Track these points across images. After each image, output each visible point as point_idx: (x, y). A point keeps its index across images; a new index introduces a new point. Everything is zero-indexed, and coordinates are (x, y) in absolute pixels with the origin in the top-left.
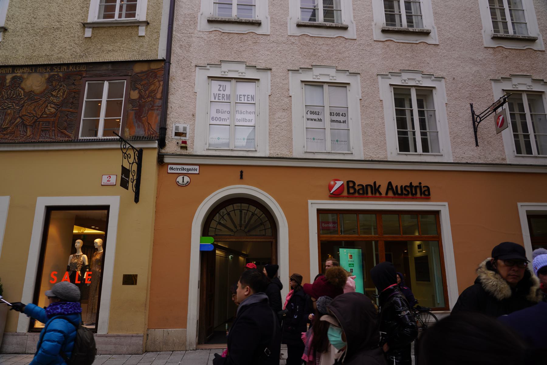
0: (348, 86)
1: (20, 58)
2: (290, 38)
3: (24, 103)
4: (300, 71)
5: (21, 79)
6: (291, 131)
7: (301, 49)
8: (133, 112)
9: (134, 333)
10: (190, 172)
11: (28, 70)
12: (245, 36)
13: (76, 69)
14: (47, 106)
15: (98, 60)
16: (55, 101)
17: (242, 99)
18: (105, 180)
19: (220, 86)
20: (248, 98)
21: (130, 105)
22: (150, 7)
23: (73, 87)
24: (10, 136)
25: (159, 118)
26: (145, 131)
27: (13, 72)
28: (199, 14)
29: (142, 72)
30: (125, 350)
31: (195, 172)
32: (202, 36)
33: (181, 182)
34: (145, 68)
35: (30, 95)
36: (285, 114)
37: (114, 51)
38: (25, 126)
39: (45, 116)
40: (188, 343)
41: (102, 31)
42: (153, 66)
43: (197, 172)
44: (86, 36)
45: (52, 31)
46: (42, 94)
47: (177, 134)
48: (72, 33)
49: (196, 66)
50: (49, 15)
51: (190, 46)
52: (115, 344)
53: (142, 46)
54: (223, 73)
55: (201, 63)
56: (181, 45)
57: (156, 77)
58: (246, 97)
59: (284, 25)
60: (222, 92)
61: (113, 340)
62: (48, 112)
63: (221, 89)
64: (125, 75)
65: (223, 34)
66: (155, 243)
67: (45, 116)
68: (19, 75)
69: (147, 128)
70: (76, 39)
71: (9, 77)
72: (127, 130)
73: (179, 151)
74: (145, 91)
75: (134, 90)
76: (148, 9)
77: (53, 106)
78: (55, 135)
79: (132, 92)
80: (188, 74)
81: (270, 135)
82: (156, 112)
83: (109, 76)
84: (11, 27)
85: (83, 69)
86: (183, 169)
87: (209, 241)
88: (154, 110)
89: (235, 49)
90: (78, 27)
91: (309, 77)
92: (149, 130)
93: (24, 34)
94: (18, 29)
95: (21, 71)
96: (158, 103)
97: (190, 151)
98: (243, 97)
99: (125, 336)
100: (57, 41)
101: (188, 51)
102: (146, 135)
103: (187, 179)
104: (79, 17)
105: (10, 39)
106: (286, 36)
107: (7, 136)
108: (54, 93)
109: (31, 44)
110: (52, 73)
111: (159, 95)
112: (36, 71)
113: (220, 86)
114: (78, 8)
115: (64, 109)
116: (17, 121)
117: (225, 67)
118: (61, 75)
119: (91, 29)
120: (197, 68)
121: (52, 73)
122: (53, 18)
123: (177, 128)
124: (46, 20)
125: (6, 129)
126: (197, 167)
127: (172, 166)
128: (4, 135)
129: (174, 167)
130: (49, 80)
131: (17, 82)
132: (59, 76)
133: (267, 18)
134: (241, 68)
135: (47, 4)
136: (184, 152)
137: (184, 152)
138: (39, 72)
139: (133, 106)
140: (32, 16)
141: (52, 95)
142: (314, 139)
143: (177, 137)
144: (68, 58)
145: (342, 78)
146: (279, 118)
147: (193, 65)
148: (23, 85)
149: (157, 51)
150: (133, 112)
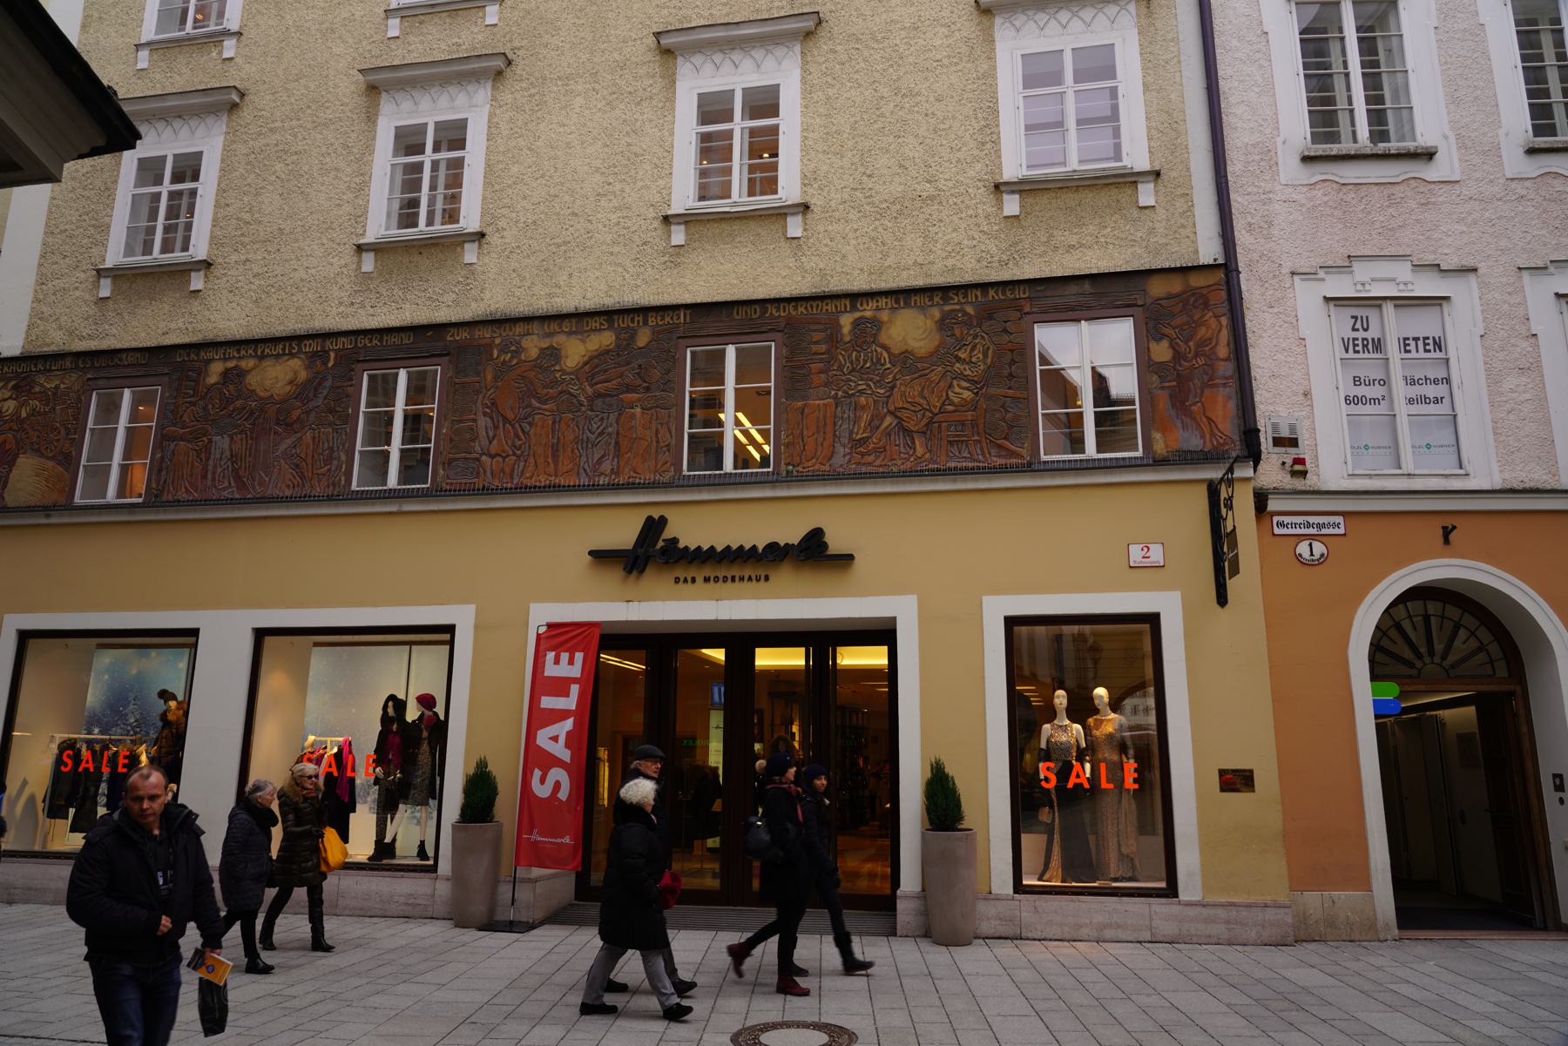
0: (1445, 304)
1: (853, 271)
2: (1514, 185)
3: (895, 379)
4: (1552, 269)
5: (877, 324)
6: (1547, 422)
7: (1545, 211)
8: (1166, 392)
9: (1268, 899)
10: (1324, 531)
11: (890, 302)
12: (1398, 188)
13: (1004, 293)
14: (951, 386)
15: (1047, 274)
16: (968, 372)
17: (1412, 347)
18: (1136, 554)
19: (1355, 318)
20: (1425, 344)
21: (1155, 377)
22: (1154, 132)
23: (1006, 338)
24: (877, 457)
25: (1232, 405)
26: (1203, 437)
27: (854, 308)
28: (1279, 141)
29: (1169, 297)
30: (1252, 935)
31: (1336, 531)
32: (1295, 196)
33: (1306, 555)
34: (1176, 285)
35: (906, 360)
36: (1524, 380)
37: (1082, 245)
38: (908, 433)
39: (950, 408)
40: (1380, 924)
41: (1044, 199)
42: (1196, 281)
43: (1342, 531)
44: (1007, 213)
45: (918, 204)
46: (934, 356)
47: (1278, 442)
48: (968, 207)
49: (1293, 273)
50: (901, 166)
51: (1270, 224)
52: (1228, 922)
53: (1152, 231)
54: (1359, 287)
55: (1303, 265)
56: (1250, 224)
57: (1206, 305)
58: (1420, 343)
59: (1495, 151)
60: (1361, 334)
61: (1220, 912)
62: (956, 400)
63: (1358, 325)
64: (1128, 306)
65: (1344, 189)
66: (1276, 700)
67: (950, 408)
68: (868, 314)
69: (1207, 431)
70: (981, 220)
71: (846, 321)
72: (1157, 436)
73: (1287, 482)
74: (1186, 343)
75: (1158, 340)
76: (1150, 139)
77: (965, 384)
78: (983, 453)
79: (1153, 345)
80: (1278, 294)
81: (1495, 434)
82: (1222, 393)
83: (1089, 308)
84: (816, 202)
85: (1022, 293)
86: (1309, 525)
87: (1391, 690)
88: (1215, 386)
89: (1378, 225)
90: (982, 194)
91: (1341, 286)
92: (1213, 435)
93: (851, 216)
94: (833, 204)
95: (872, 304)
96: (1226, 369)
97: (1311, 481)
98: (1413, 343)
99: (1249, 906)
100: (935, 229)
101: (1268, 238)
102: (1208, 447)
103: (1319, 548)
104: (979, 166)
105: (821, 228)
106: (1502, 181)
107: (871, 458)
108: (962, 355)
109: (873, 239)
110: (947, 308)
111: (1223, 351)
112: (907, 305)
113: (1355, 318)
114: (972, 144)
115: (992, 390)
116: (886, 424)
117: (1362, 271)
118: (970, 310)
119: (1017, 196)
120: (1296, 278)
121: (947, 308)
122: (914, 173)
123: (1275, 427)
124: (897, 179)
125: (863, 441)
126: (1340, 519)
127: (1281, 518)
128: (863, 455)
129: (1287, 519)
130: (943, 324)
131: (867, 331)
132: (965, 313)
133: (1446, 137)
134: (1403, 271)
135: (891, 139)
136: (1299, 484)
137: (1299, 484)
138: (915, 306)
139: (1162, 379)
140: (861, 169)
141: (958, 359)
142: (1428, 446)
143: (1278, 449)
144: (969, 269)
145: (1427, 286)
146: (1512, 391)
147: (1286, 270)
148: (883, 338)
149: (1194, 242)
150: (1166, 392)
